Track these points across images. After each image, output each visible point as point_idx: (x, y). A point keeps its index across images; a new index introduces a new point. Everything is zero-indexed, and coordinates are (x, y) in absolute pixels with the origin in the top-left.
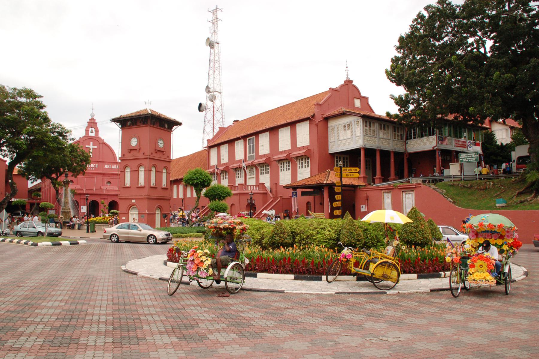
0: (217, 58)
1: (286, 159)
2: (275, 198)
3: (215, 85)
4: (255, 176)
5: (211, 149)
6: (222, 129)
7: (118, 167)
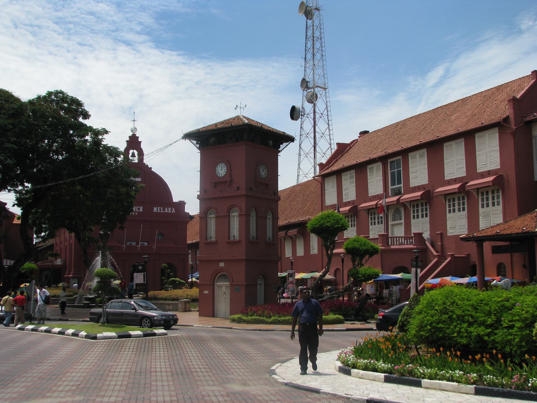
0: (317, 34)
1: (459, 192)
2: (442, 257)
3: (317, 77)
4: (403, 221)
5: (326, 179)
6: (342, 149)
7: (174, 211)
